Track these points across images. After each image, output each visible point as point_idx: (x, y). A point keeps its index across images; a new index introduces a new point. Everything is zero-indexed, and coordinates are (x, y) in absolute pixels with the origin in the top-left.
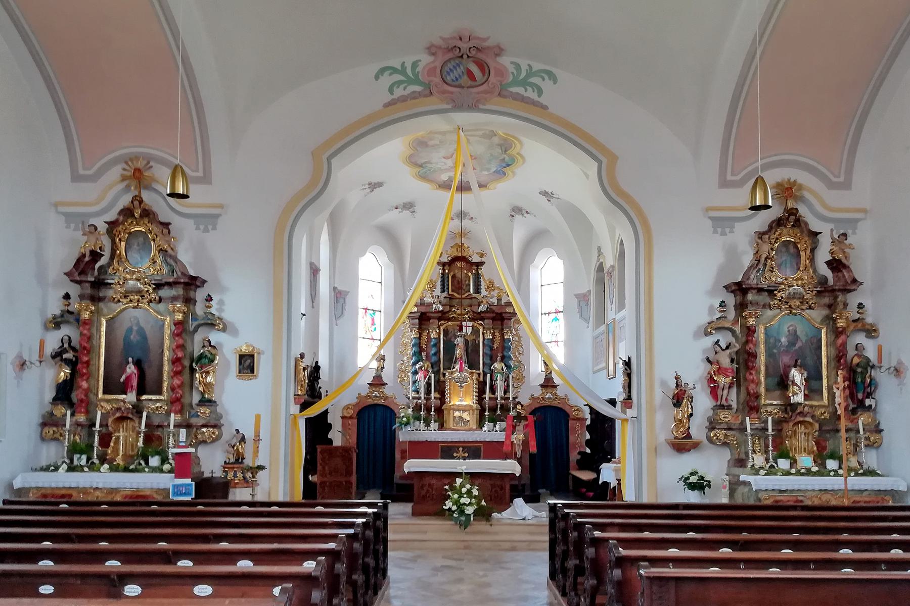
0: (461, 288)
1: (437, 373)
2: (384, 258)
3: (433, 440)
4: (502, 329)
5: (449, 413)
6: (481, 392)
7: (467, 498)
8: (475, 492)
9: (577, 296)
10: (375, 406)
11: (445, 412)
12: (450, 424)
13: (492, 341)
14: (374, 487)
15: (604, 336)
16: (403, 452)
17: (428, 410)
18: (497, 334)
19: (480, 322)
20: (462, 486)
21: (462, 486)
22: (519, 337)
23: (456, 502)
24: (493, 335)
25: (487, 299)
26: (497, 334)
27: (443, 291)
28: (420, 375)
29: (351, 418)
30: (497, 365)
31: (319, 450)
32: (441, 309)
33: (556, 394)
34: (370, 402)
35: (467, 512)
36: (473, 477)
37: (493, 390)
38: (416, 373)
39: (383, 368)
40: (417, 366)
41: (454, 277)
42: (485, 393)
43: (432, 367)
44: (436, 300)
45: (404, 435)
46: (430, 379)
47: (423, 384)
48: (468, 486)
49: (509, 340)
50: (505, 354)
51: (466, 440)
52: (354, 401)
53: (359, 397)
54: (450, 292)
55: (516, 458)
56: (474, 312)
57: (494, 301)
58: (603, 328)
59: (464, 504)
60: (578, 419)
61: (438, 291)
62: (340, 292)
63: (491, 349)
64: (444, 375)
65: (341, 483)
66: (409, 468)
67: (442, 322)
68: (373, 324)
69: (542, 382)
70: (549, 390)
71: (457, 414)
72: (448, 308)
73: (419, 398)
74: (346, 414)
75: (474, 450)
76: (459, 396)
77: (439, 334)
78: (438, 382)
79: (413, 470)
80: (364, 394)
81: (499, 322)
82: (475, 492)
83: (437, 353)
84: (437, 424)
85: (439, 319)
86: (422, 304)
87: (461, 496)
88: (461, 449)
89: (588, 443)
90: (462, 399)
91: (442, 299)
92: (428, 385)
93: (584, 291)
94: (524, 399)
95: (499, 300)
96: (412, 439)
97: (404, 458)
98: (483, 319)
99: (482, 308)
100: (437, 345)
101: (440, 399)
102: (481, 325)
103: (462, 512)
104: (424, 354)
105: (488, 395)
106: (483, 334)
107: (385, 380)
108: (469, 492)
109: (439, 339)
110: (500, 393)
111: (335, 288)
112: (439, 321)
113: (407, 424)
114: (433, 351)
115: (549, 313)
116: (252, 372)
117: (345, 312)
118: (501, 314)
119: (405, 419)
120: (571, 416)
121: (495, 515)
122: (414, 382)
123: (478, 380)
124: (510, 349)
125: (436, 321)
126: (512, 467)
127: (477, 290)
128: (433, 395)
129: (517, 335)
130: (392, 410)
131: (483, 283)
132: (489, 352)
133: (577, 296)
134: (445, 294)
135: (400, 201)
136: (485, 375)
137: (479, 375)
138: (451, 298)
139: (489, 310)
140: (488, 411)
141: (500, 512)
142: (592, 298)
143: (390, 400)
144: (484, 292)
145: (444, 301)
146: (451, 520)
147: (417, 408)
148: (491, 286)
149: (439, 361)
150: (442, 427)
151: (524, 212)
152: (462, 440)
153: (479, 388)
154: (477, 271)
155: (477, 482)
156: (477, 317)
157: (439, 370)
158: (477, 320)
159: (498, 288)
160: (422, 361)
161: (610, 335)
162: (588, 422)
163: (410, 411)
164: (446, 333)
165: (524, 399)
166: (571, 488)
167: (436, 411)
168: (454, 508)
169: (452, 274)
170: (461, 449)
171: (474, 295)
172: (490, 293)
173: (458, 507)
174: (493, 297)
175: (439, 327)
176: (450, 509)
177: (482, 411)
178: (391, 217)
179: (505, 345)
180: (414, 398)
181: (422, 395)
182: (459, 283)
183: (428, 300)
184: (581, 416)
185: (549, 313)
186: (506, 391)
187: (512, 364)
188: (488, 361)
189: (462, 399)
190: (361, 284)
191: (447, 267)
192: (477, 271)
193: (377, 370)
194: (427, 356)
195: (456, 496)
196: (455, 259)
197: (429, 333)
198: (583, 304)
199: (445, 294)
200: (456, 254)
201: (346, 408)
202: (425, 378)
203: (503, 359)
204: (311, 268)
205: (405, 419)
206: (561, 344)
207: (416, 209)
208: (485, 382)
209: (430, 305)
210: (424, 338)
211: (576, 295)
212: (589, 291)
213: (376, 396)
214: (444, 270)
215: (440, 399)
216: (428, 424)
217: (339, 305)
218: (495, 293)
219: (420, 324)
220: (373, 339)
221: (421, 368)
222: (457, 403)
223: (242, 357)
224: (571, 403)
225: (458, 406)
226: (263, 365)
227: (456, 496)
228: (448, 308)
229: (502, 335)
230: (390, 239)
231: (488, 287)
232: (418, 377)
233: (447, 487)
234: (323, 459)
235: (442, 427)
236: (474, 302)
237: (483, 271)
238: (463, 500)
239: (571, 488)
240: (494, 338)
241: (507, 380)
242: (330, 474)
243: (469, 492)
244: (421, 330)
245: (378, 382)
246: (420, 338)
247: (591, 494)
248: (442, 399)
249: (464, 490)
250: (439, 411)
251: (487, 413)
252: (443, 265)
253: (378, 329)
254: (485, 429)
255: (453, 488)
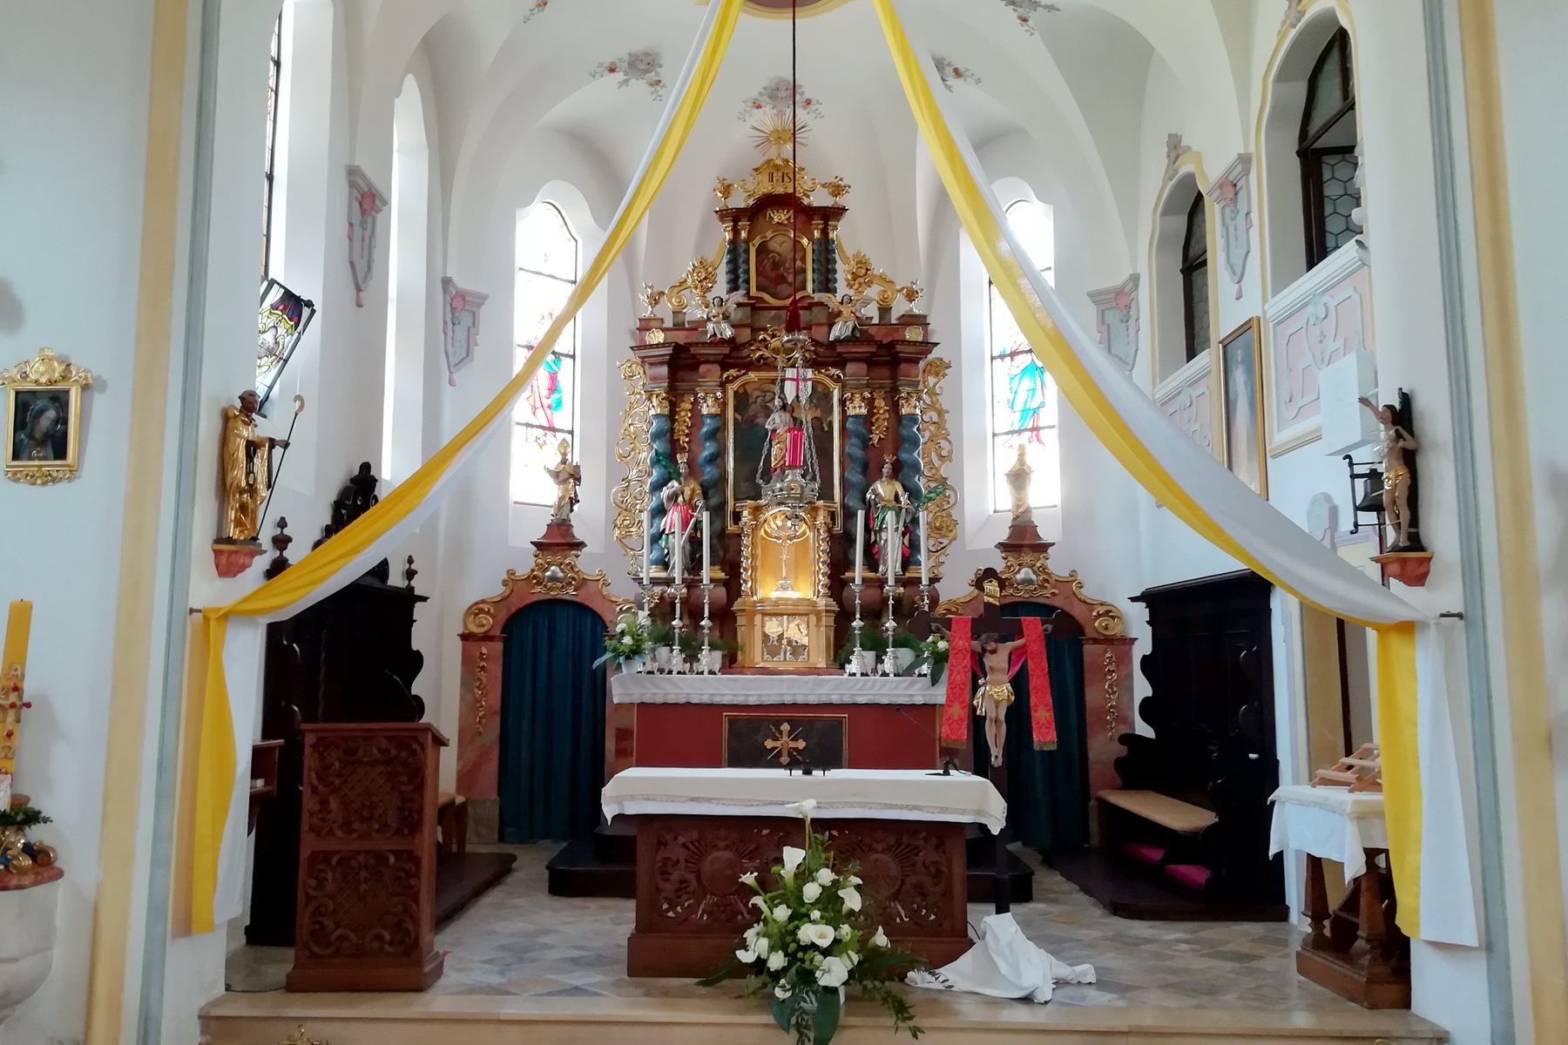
0: (782, 279)
1: (718, 511)
2: (582, 217)
3: (706, 700)
4: (895, 390)
5: (751, 624)
6: (839, 566)
7: (818, 922)
8: (852, 900)
9: (1095, 297)
10: (550, 606)
11: (741, 620)
12: (756, 654)
13: (868, 420)
14: (546, 836)
15: (1216, 382)
16: (624, 734)
17: (693, 613)
18: (880, 403)
19: (834, 371)
20: (805, 874)
21: (805, 874)
22: (940, 413)
23: (785, 939)
24: (870, 403)
25: (853, 305)
26: (880, 403)
27: (734, 286)
28: (674, 517)
29: (486, 637)
30: (883, 489)
31: (310, 739)
32: (728, 333)
33: (1044, 569)
34: (539, 593)
35: (824, 980)
36: (847, 839)
37: (872, 560)
38: (660, 511)
39: (574, 501)
40: (665, 492)
41: (763, 250)
42: (850, 565)
43: (705, 496)
44: (710, 310)
45: (628, 686)
46: (698, 526)
47: (677, 543)
48: (826, 876)
49: (913, 419)
50: (904, 456)
51: (800, 700)
52: (496, 590)
53: (511, 580)
54: (753, 292)
55: (980, 766)
56: (815, 343)
57: (872, 312)
58: (1208, 359)
59: (813, 946)
60: (1109, 641)
61: (721, 287)
62: (462, 296)
63: (865, 443)
64: (737, 517)
65: (381, 858)
66: (619, 800)
67: (733, 372)
68: (553, 388)
69: (1003, 535)
70: (1027, 558)
71: (773, 627)
72: (746, 335)
73: (669, 582)
74: (474, 629)
75: (823, 738)
76: (778, 576)
77: (724, 405)
78: (720, 536)
79: (632, 809)
80: (522, 571)
81: (885, 372)
82: (852, 900)
83: (717, 458)
84: (718, 655)
85: (725, 366)
86: (678, 326)
87: (800, 916)
88: (785, 727)
89: (1147, 709)
90: (786, 581)
91: (731, 306)
92: (695, 543)
93: (1118, 279)
94: (955, 588)
95: (885, 310)
96: (648, 700)
97: (626, 758)
98: (841, 364)
99: (838, 331)
100: (716, 434)
101: (726, 583)
102: (837, 379)
103: (806, 978)
104: (682, 459)
105: (859, 572)
106: (843, 403)
107: (579, 533)
108: (830, 899)
109: (721, 416)
110: (891, 564)
111: (447, 282)
112: (725, 368)
113: (635, 652)
114: (709, 449)
115: (1013, 354)
116: (60, 453)
117: (477, 351)
118: (892, 345)
119: (627, 640)
120: (1090, 633)
121: (917, 978)
122: (655, 539)
123: (829, 531)
124: (916, 443)
125: (716, 368)
126: (971, 799)
127: (826, 283)
128: (706, 573)
129: (932, 406)
130: (597, 618)
131: (839, 266)
132: (858, 453)
133: (1095, 297)
134: (739, 296)
135: (620, 50)
136: (849, 515)
137: (833, 515)
138: (755, 306)
139: (861, 334)
140: (865, 612)
141: (933, 965)
142: (1145, 299)
143: (591, 587)
144: (842, 288)
145: (736, 315)
146: (762, 1009)
147: (663, 610)
148: (863, 273)
149: (723, 478)
150: (731, 663)
151: (949, 71)
152: (788, 700)
153: (832, 553)
154: (825, 232)
155: (855, 865)
156: (826, 356)
157: (724, 504)
158: (825, 365)
159: (882, 278)
160: (678, 477)
161: (1239, 376)
162: (1143, 645)
163: (643, 617)
164: (742, 400)
165: (955, 588)
166: (1095, 840)
167: (710, 613)
168: (777, 961)
169: (757, 241)
170: (785, 727)
171: (818, 297)
172: (858, 292)
173: (792, 957)
174: (866, 303)
175: (723, 385)
176: (760, 964)
177: (843, 617)
178: (597, 99)
179: (901, 435)
180: (655, 582)
181: (677, 574)
182: (776, 266)
183: (696, 312)
184: (1116, 630)
185: (1013, 354)
186: (908, 561)
187: (922, 483)
188: (856, 477)
189: (786, 581)
190: (520, 278)
191: (743, 223)
192: (825, 232)
193: (560, 507)
194: (690, 464)
195: (782, 913)
196: (768, 202)
197: (695, 403)
198: (1113, 317)
199: (739, 296)
200: (766, 188)
201: (476, 610)
202: (685, 524)
203: (897, 471)
204: (352, 185)
205: (627, 640)
206: (1051, 437)
207: (664, 73)
208: (848, 538)
209: (698, 326)
210: (684, 416)
211: (1092, 295)
212: (1135, 279)
213: (553, 579)
214: (736, 232)
215: (726, 583)
216: (691, 656)
217: (461, 332)
218: (873, 292)
219: (673, 378)
220: (552, 429)
221: (673, 497)
222: (774, 595)
223: (26, 406)
224: (1089, 593)
225: (777, 602)
226: (100, 433)
227: (782, 913)
228: (746, 335)
229: (895, 407)
230: (596, 162)
231: (855, 276)
232: (664, 523)
233: (749, 879)
234: (323, 772)
235: (731, 663)
236: (819, 315)
237: (841, 232)
238: (810, 933)
239: (1095, 840)
240: (871, 413)
241: (910, 528)
242: (346, 826)
243: (830, 899)
244: (674, 396)
245: (559, 540)
246: (672, 416)
247: (1327, 932)
248: (732, 583)
249: (811, 891)
250: (725, 617)
251: (857, 623)
252: (734, 216)
253: (567, 399)
254: (853, 667)
255: (767, 883)
